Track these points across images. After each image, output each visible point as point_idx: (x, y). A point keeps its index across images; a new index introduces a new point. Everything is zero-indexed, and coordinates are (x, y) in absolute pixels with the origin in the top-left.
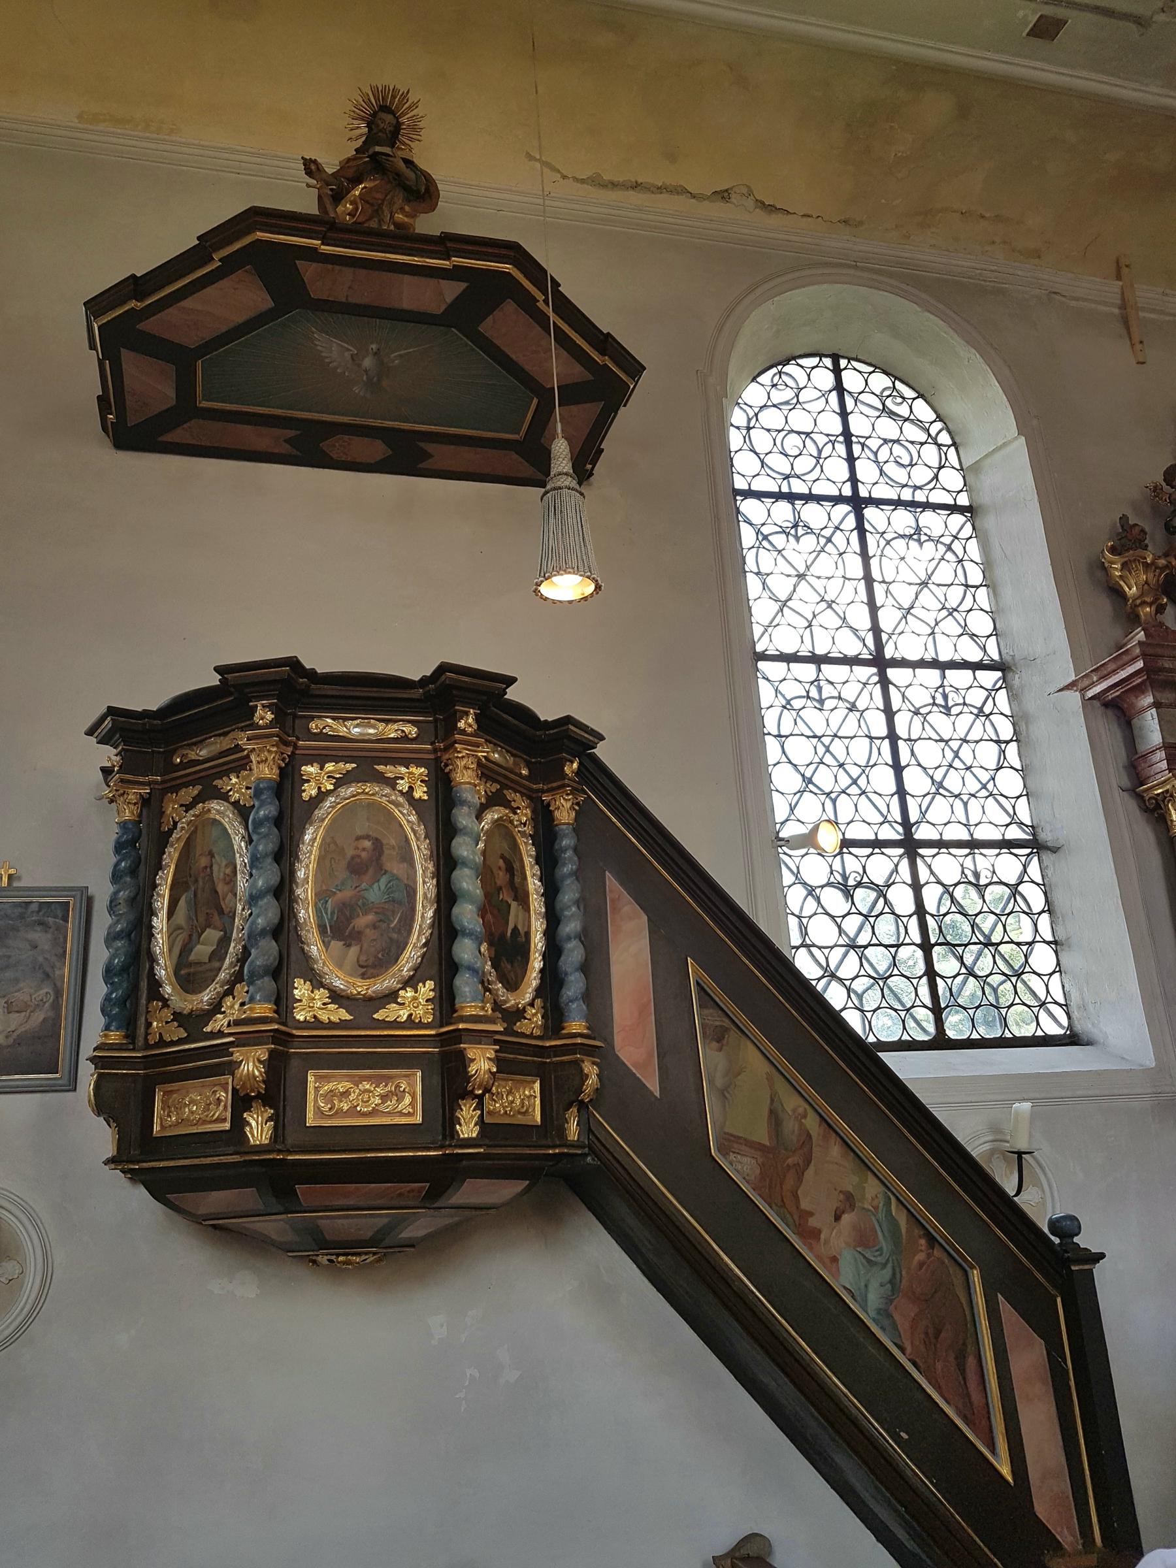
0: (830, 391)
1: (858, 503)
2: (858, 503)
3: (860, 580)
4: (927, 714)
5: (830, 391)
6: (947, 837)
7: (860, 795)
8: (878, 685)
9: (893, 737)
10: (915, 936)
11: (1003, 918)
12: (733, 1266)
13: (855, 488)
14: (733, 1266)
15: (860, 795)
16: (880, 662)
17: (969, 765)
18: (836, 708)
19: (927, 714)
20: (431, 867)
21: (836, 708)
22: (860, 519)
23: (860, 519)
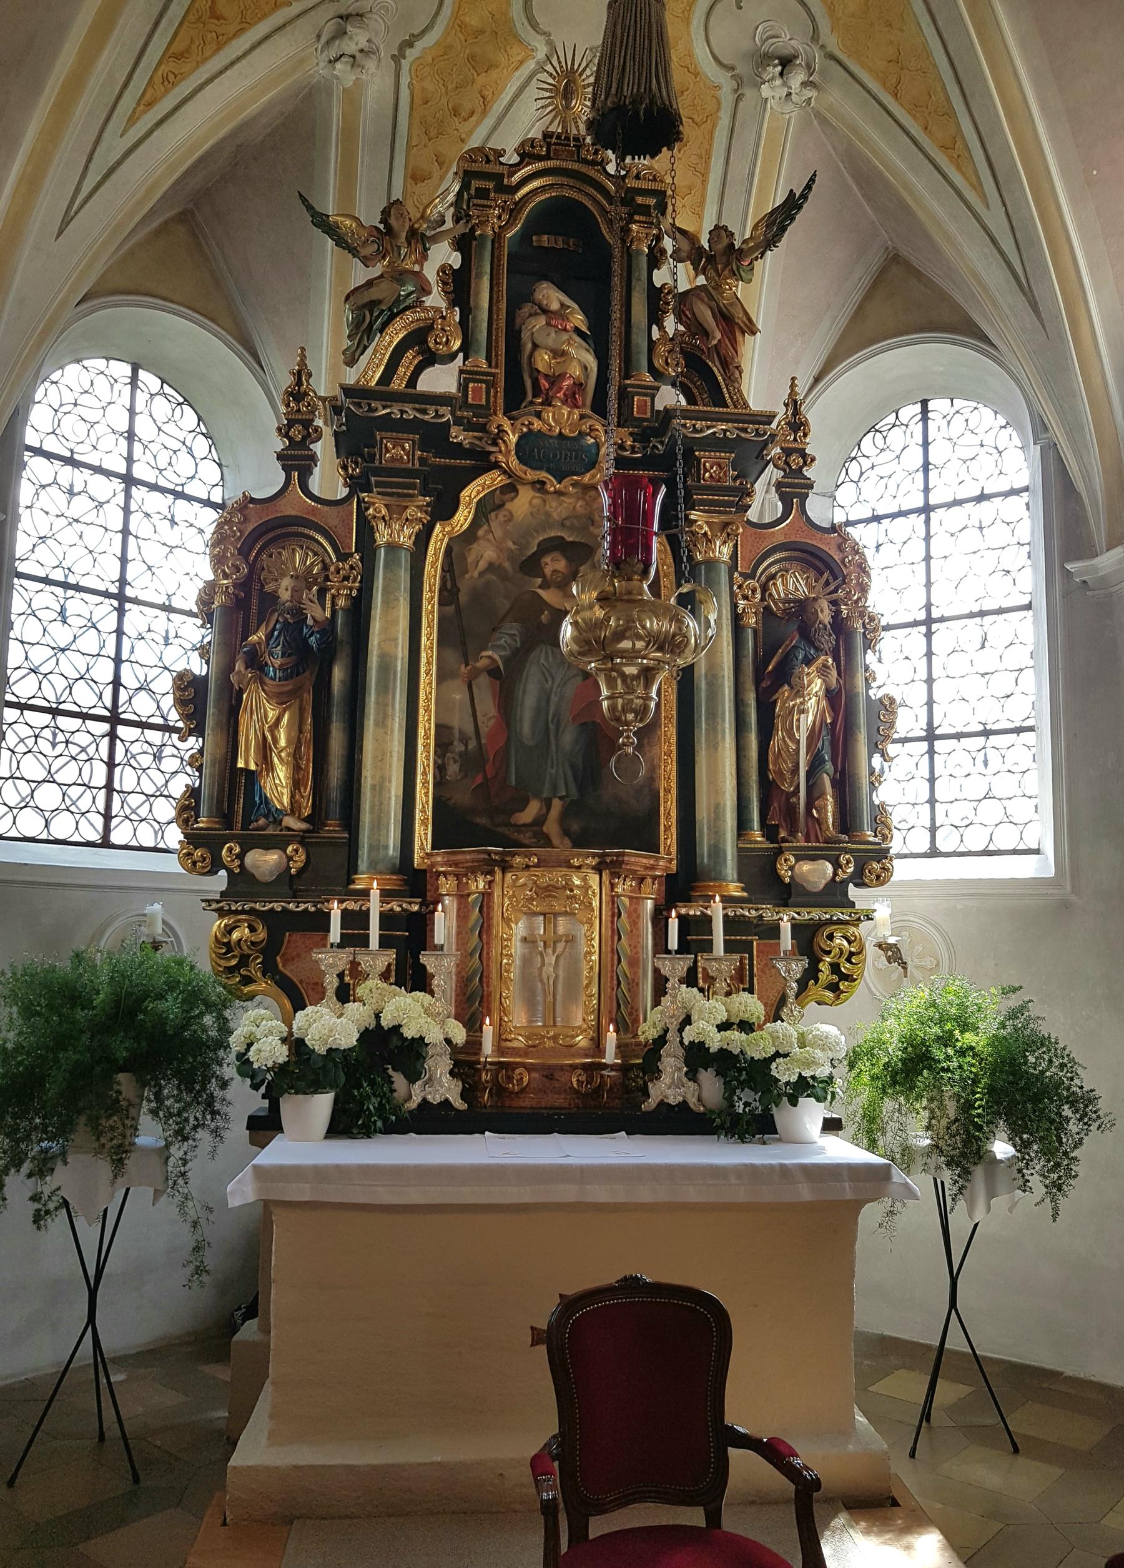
0: (103, 736)
1: (129, 481)
2: (129, 481)
3: (100, 789)
4: (130, 765)
5: (103, 736)
6: (137, 731)
7: (67, 746)
8: (111, 685)
9: (125, 532)
10: (111, 650)
11: (152, 799)
12: (703, 704)
13: (122, 588)
14: (703, 704)
15: (67, 746)
16: (121, 598)
17: (143, 817)
18: (69, 412)
19: (130, 765)
20: (360, 853)
21: (69, 412)
22: (128, 497)
23: (128, 497)
